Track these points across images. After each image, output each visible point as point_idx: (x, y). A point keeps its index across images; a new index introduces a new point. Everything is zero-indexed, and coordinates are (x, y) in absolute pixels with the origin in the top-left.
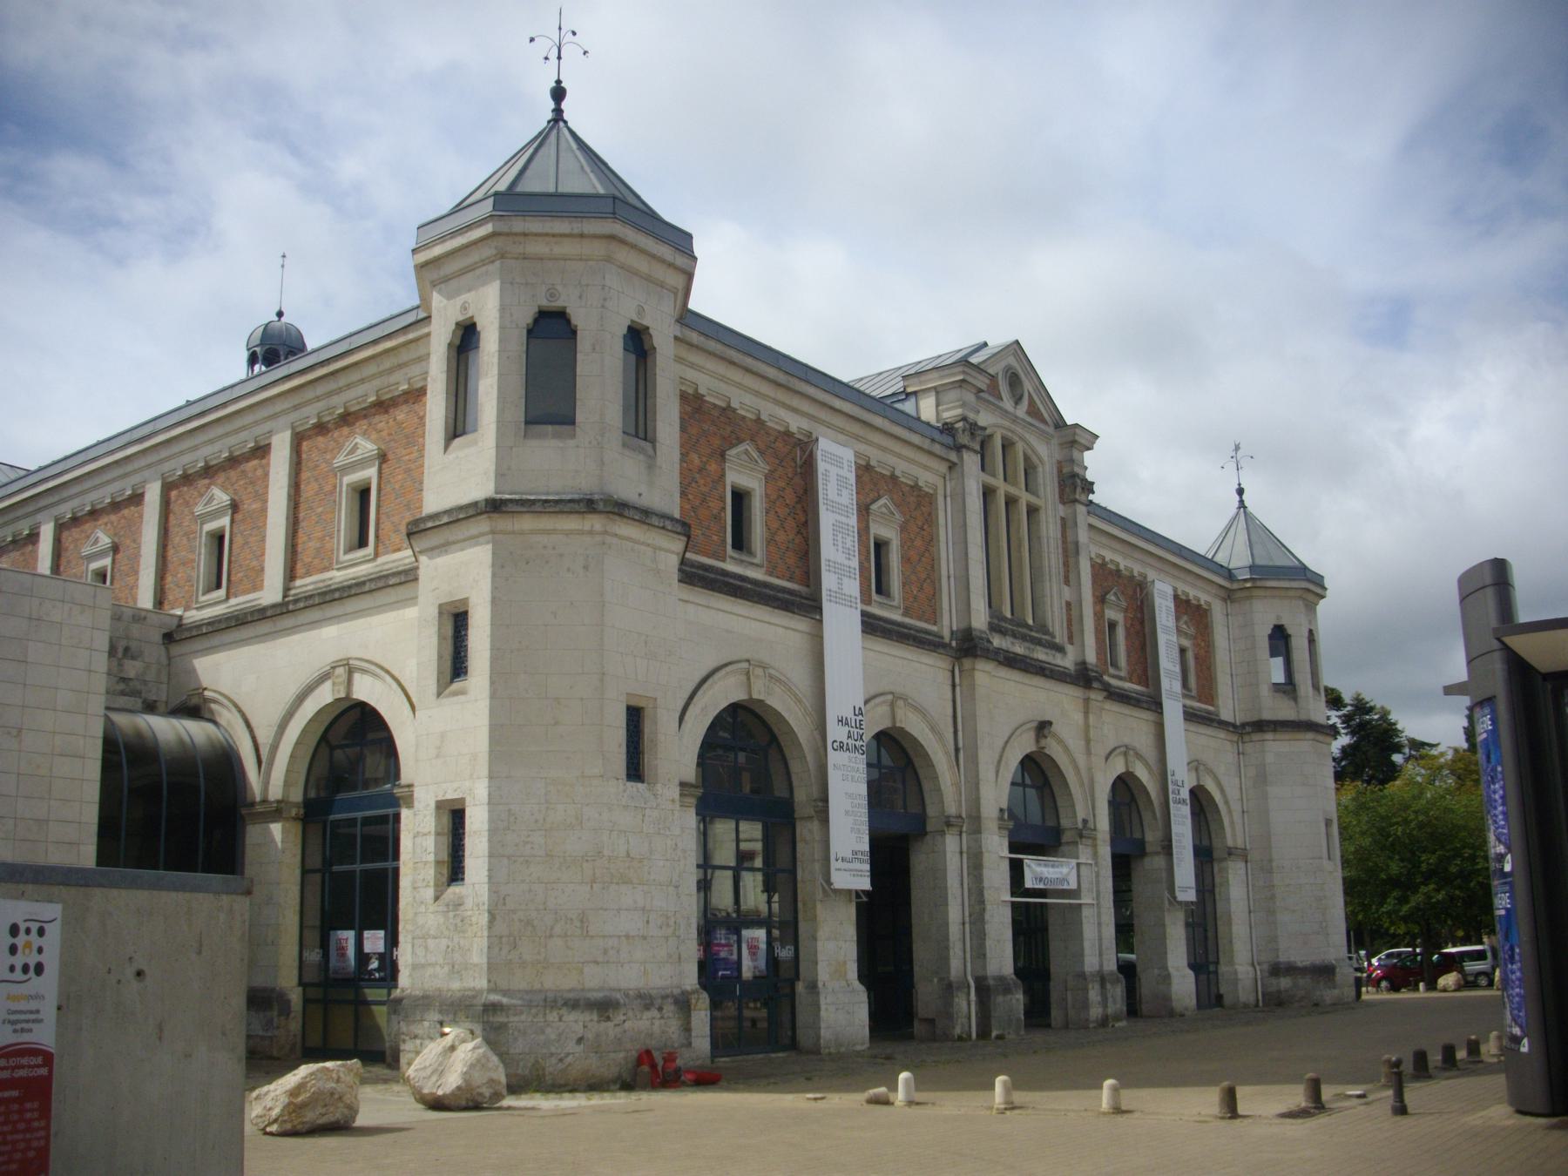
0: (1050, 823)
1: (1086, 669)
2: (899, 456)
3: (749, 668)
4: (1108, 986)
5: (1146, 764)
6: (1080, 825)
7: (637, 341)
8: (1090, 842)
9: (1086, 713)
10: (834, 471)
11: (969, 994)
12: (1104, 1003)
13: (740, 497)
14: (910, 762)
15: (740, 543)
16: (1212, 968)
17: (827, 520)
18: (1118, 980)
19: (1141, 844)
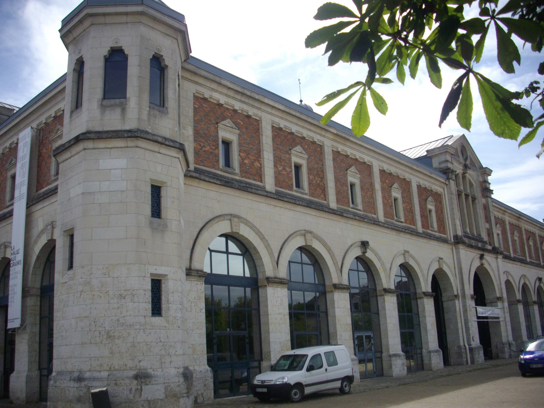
2: (315, 132)
3: (305, 233)
5: (449, 267)
7: (157, 63)
13: (227, 144)
15: (298, 185)
16: (419, 351)
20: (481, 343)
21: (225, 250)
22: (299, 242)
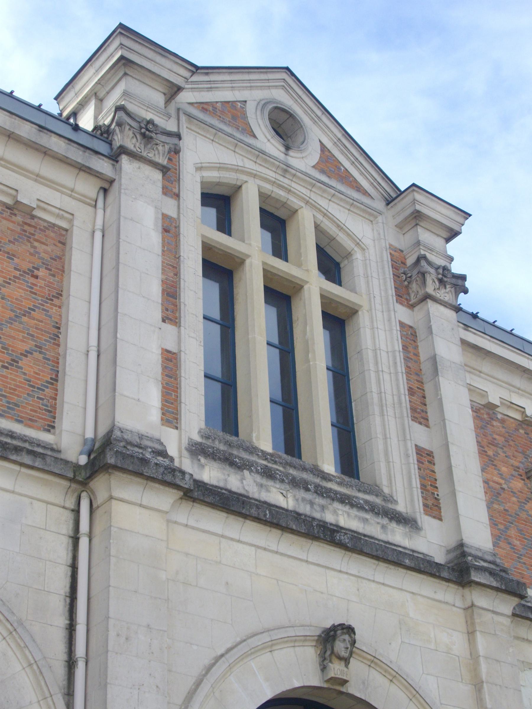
1: (464, 554)
9: (471, 634)
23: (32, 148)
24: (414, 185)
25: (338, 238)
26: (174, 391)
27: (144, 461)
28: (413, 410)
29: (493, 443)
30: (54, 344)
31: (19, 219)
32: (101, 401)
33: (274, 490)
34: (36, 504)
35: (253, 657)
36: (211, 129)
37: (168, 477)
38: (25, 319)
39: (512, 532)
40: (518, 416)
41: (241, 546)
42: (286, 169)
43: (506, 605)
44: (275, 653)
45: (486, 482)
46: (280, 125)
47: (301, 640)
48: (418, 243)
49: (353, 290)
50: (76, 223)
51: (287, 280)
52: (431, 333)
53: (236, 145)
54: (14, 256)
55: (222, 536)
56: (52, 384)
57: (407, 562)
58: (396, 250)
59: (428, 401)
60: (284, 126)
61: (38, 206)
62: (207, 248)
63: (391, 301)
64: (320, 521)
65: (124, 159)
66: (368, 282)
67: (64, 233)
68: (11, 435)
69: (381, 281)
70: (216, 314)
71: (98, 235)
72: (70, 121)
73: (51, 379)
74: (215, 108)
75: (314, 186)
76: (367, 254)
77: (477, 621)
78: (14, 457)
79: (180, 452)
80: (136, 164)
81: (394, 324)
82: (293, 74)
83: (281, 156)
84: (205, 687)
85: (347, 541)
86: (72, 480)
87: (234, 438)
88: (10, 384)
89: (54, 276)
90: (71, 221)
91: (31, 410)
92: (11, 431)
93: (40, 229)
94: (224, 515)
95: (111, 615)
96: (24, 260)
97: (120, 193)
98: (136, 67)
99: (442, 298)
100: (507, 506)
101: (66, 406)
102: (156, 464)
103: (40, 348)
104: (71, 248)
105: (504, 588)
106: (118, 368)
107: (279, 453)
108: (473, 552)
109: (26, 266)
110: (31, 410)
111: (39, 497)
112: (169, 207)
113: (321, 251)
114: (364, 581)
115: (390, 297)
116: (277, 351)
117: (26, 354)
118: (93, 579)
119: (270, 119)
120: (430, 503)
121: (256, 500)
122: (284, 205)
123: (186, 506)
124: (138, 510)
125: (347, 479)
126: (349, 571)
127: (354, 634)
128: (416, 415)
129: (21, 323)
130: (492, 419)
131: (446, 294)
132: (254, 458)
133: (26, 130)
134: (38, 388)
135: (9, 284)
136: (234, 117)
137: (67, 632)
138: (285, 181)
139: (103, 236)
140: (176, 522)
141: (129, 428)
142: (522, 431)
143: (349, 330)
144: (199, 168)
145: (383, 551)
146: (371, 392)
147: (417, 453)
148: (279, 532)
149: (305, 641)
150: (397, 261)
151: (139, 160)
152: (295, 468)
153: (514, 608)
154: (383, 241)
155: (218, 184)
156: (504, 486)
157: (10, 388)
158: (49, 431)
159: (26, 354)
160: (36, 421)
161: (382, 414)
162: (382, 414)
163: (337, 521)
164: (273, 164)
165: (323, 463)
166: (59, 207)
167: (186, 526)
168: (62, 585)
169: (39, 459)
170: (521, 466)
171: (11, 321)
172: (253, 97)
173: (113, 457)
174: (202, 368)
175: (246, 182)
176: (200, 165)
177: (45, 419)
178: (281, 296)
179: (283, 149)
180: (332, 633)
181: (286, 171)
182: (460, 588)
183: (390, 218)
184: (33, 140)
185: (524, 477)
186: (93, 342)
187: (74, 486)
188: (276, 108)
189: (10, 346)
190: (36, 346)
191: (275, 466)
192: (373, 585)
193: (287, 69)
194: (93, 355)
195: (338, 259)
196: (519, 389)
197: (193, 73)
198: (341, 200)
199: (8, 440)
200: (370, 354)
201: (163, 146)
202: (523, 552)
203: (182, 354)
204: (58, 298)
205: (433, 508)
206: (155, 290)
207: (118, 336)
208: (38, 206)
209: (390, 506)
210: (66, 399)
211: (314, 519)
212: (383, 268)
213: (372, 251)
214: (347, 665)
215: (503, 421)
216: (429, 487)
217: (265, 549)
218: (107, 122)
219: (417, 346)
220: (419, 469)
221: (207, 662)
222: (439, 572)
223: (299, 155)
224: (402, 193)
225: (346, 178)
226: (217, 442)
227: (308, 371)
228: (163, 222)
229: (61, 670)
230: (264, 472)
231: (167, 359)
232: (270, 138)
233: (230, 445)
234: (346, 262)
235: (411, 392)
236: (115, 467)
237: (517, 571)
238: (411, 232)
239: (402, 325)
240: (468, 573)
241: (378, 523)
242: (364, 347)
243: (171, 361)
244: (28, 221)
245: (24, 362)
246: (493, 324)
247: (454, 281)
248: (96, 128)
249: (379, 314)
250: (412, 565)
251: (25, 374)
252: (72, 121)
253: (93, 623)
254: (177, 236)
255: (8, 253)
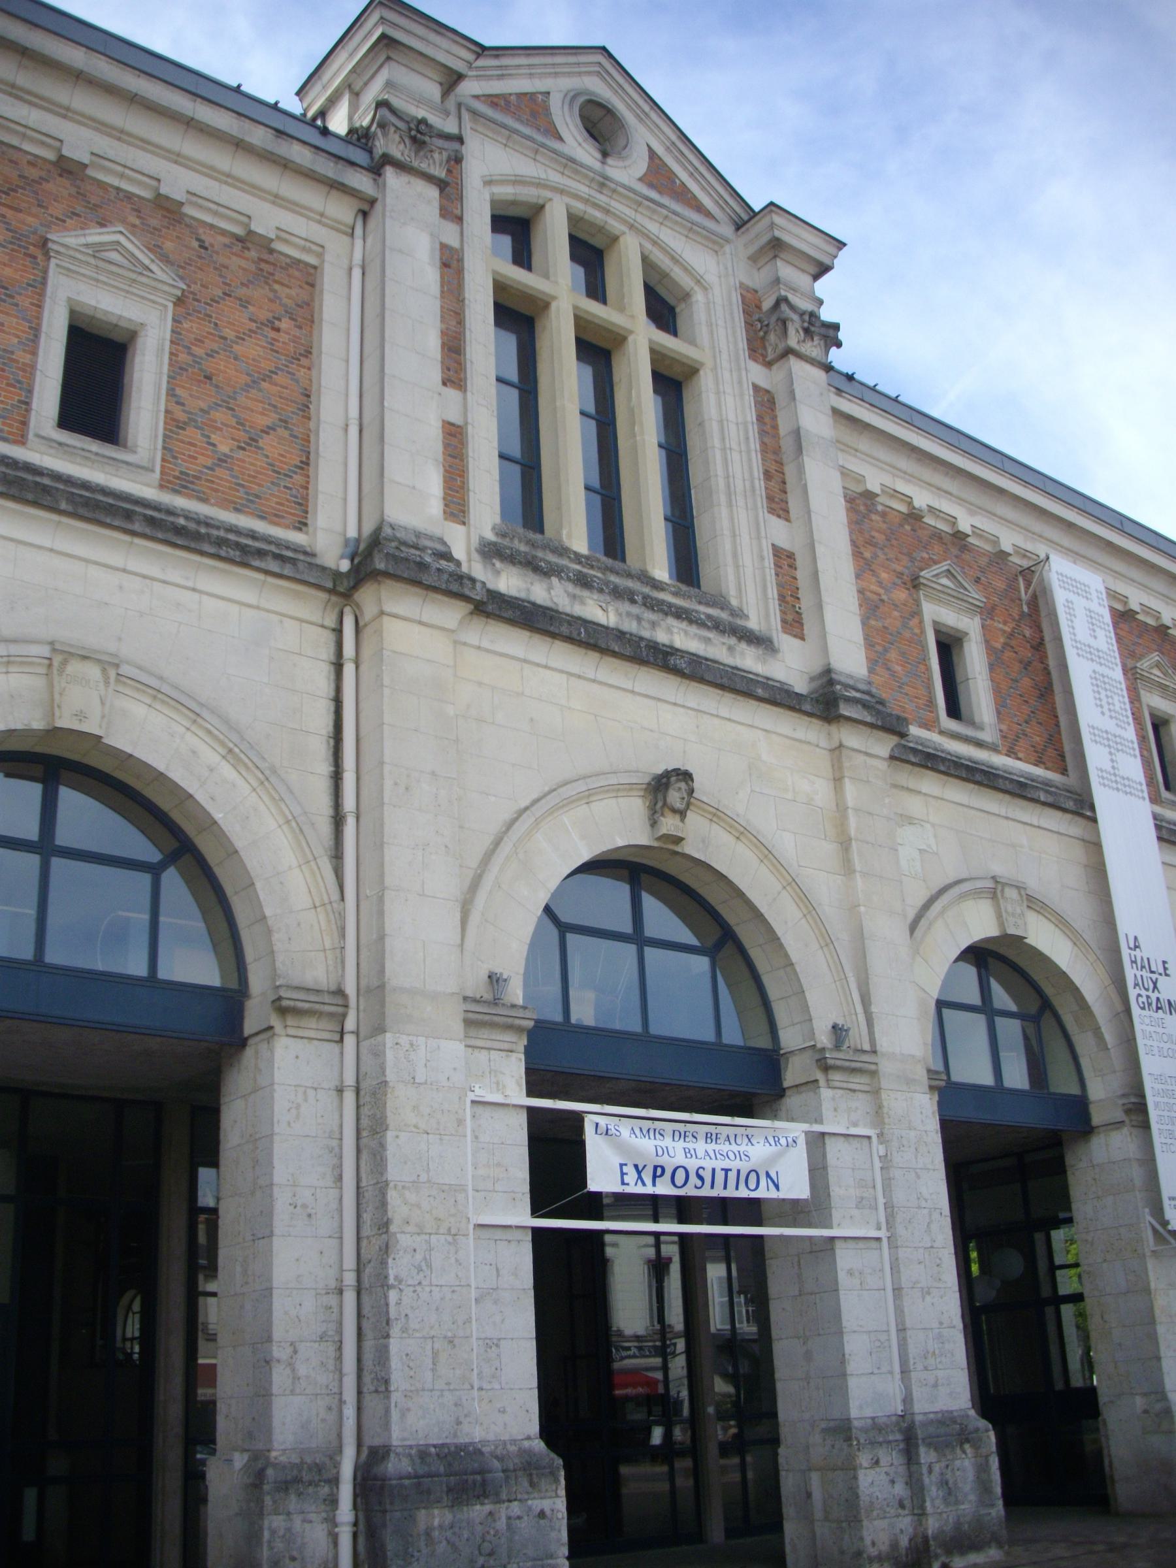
0: (763, 1043)
1: (831, 682)
4: (926, 1456)
5: (1061, 922)
6: (824, 1039)
8: (858, 1082)
9: (838, 781)
10: (1080, 603)
11: (333, 1502)
12: (916, 1502)
14: (1046, 1005)
17: (1081, 673)
18: (965, 1437)
19: (1079, 1106)
20: (550, 1429)
21: (627, 928)
22: (980, 924)
23: (268, 160)
24: (772, 204)
25: (672, 274)
26: (460, 476)
27: (422, 566)
28: (770, 499)
29: (871, 543)
30: (303, 417)
31: (253, 254)
32: (366, 490)
33: (591, 602)
34: (288, 623)
35: (566, 809)
36: (503, 130)
37: (452, 585)
38: (265, 385)
39: (893, 655)
40: (903, 508)
41: (548, 672)
42: (603, 183)
43: (883, 745)
44: (593, 805)
45: (861, 592)
46: (595, 125)
47: (625, 790)
48: (777, 281)
49: (692, 342)
50: (327, 257)
51: (606, 329)
52: (794, 399)
53: (537, 152)
54: (248, 303)
55: (525, 661)
56: (302, 469)
57: (760, 692)
58: (748, 289)
59: (789, 487)
60: (600, 124)
61: (278, 237)
62: (500, 287)
63: (742, 357)
64: (650, 641)
65: (389, 172)
66: (712, 333)
67: (312, 271)
68: (253, 535)
69: (730, 331)
70: (513, 375)
71: (357, 273)
72: (317, 123)
73: (302, 462)
74: (508, 102)
75: (640, 204)
76: (710, 296)
77: (846, 764)
78: (256, 563)
79: (469, 554)
80: (405, 178)
81: (745, 386)
82: (611, 56)
83: (597, 165)
84: (506, 848)
85: (684, 666)
86: (332, 591)
87: (538, 536)
88: (249, 469)
89: (300, 328)
90: (320, 256)
91: (278, 503)
92: (252, 531)
93: (281, 267)
94: (527, 634)
95: (387, 759)
96: (261, 308)
97: (384, 215)
98: (401, 48)
99: (808, 353)
100: (887, 623)
101: (321, 497)
102: (439, 570)
103: (286, 422)
104: (322, 291)
105: (880, 723)
106: (386, 447)
107: (597, 555)
108: (843, 679)
109: (264, 315)
110: (278, 503)
111: (290, 613)
112: (449, 234)
113: (649, 290)
114: (705, 716)
115: (741, 352)
116: (593, 423)
117: (267, 430)
118: (362, 715)
119: (581, 116)
120: (790, 618)
121: (568, 615)
122: (601, 229)
123: (478, 623)
124: (417, 628)
125: (684, 588)
126: (687, 704)
127: (692, 780)
128: (773, 506)
129: (260, 390)
130: (870, 511)
131: (812, 349)
132: (564, 562)
133: (258, 136)
134: (286, 475)
135: (243, 339)
136: (534, 114)
137: (332, 781)
138: (602, 199)
139: (363, 274)
140: (465, 644)
141: (402, 523)
142: (908, 528)
143: (687, 395)
144: (488, 183)
145: (730, 679)
146: (716, 476)
147: (775, 555)
148: (597, 655)
149: (631, 789)
150: (750, 304)
151: (409, 173)
152: (618, 574)
153: (892, 750)
154: (731, 279)
155: (514, 203)
156: (884, 597)
157: (249, 476)
158: (300, 529)
159: (267, 430)
160: (283, 517)
161: (730, 505)
162: (730, 505)
163: (672, 641)
164: (586, 176)
165: (654, 567)
166: (304, 236)
167: (479, 648)
168: (322, 722)
169: (288, 565)
170: (906, 571)
171: (247, 387)
172: (558, 87)
173: (383, 560)
174: (495, 444)
175: (550, 200)
176: (488, 178)
177: (297, 516)
178: (598, 351)
179: (598, 156)
180: (664, 780)
181: (603, 185)
182: (826, 725)
183: (741, 247)
184: (269, 148)
185: (909, 585)
186: (354, 412)
187: (334, 598)
188: (590, 102)
189: (246, 420)
190: (280, 420)
191: (592, 572)
192: (716, 721)
193: (604, 49)
194: (354, 430)
195: (671, 301)
196: (905, 473)
197: (478, 56)
198: (676, 223)
199: (249, 542)
200: (715, 426)
201: (440, 153)
202: (905, 679)
203: (470, 427)
204: (307, 357)
205: (794, 624)
206: (433, 343)
207: (386, 404)
208: (278, 237)
209: (739, 622)
210: (320, 488)
211: (641, 638)
212: (732, 314)
213: (717, 291)
214: (682, 820)
215: (884, 515)
216: (789, 599)
217: (579, 677)
218: (365, 123)
219: (776, 417)
220: (777, 575)
221: (507, 816)
222: (799, 704)
223: (621, 164)
224: (755, 214)
225: (683, 195)
226: (516, 541)
227: (634, 450)
228: (442, 254)
229: (325, 827)
230: (578, 580)
231: (450, 435)
232: (581, 140)
233: (533, 545)
234: (683, 306)
235: (768, 475)
236: (386, 574)
237: (897, 703)
238: (768, 267)
239: (756, 388)
240: (837, 706)
241: (724, 644)
242: (706, 417)
243: (455, 437)
244: (265, 256)
245: (265, 441)
246: (873, 389)
247: (823, 331)
248: (351, 131)
249: (727, 375)
250: (767, 696)
251: (267, 457)
252: (319, 122)
253: (364, 769)
254: (460, 272)
255: (240, 300)
